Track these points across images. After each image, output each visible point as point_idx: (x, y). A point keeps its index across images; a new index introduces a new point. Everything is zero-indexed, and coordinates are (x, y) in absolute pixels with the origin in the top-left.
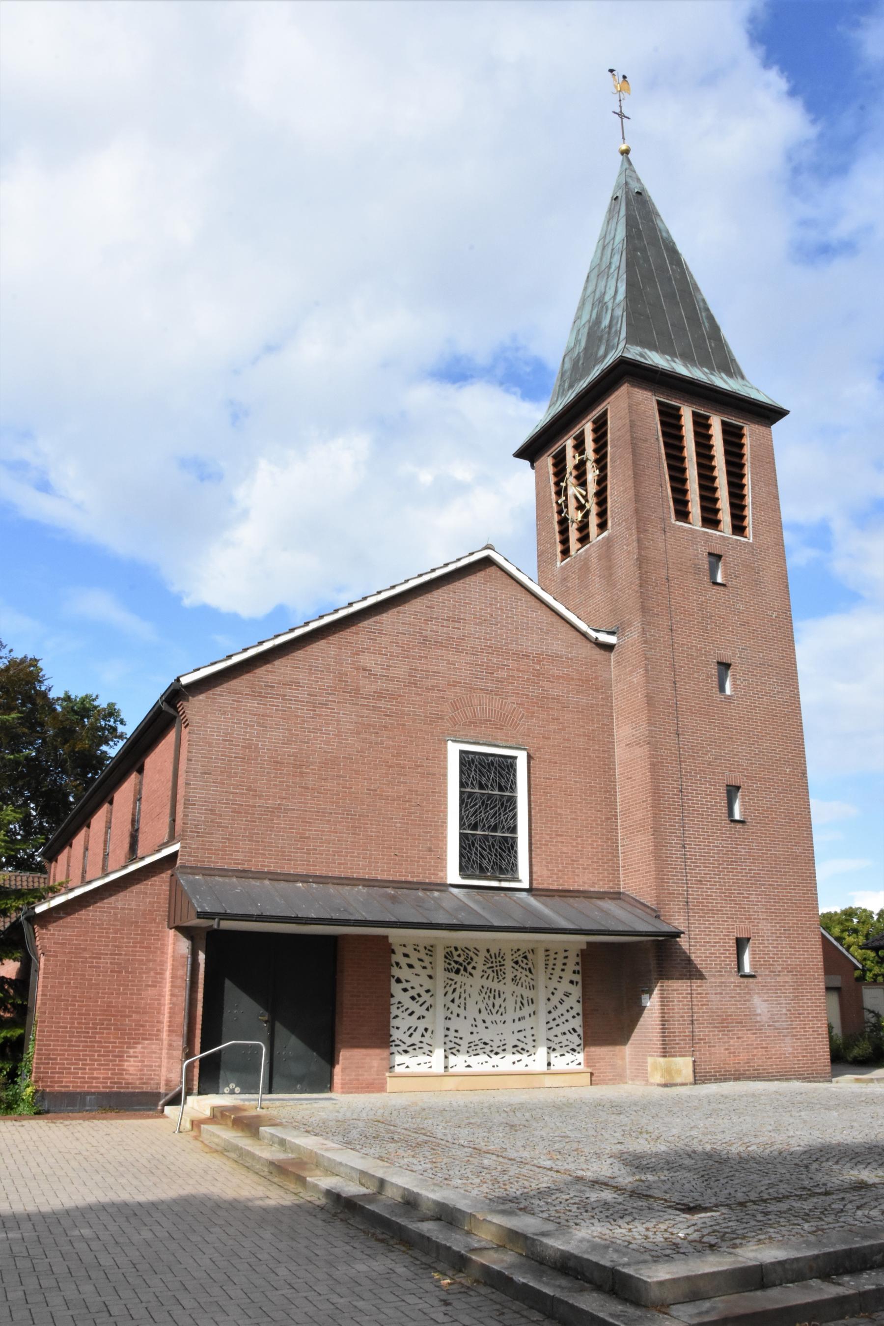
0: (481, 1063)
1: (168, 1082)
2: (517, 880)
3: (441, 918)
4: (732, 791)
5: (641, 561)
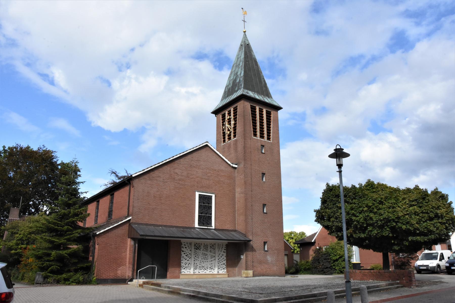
0: (202, 272)
1: (128, 276)
2: (212, 227)
3: (195, 236)
4: (264, 205)
5: (244, 147)
